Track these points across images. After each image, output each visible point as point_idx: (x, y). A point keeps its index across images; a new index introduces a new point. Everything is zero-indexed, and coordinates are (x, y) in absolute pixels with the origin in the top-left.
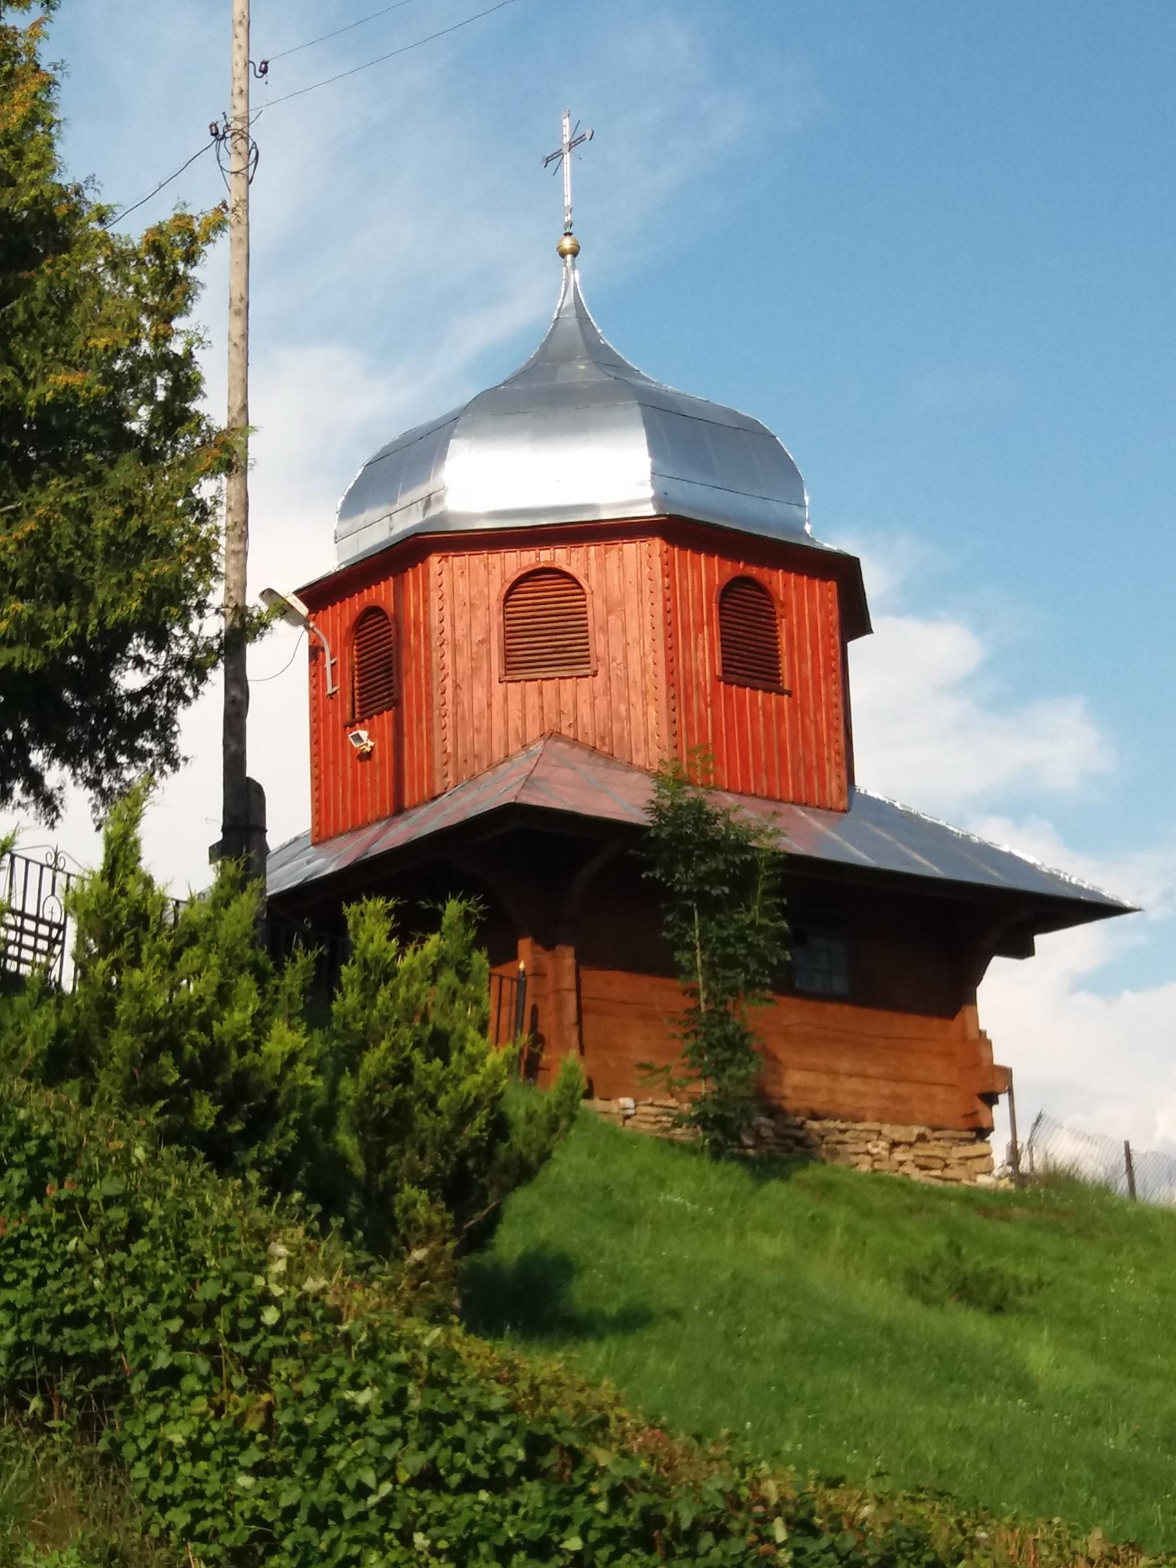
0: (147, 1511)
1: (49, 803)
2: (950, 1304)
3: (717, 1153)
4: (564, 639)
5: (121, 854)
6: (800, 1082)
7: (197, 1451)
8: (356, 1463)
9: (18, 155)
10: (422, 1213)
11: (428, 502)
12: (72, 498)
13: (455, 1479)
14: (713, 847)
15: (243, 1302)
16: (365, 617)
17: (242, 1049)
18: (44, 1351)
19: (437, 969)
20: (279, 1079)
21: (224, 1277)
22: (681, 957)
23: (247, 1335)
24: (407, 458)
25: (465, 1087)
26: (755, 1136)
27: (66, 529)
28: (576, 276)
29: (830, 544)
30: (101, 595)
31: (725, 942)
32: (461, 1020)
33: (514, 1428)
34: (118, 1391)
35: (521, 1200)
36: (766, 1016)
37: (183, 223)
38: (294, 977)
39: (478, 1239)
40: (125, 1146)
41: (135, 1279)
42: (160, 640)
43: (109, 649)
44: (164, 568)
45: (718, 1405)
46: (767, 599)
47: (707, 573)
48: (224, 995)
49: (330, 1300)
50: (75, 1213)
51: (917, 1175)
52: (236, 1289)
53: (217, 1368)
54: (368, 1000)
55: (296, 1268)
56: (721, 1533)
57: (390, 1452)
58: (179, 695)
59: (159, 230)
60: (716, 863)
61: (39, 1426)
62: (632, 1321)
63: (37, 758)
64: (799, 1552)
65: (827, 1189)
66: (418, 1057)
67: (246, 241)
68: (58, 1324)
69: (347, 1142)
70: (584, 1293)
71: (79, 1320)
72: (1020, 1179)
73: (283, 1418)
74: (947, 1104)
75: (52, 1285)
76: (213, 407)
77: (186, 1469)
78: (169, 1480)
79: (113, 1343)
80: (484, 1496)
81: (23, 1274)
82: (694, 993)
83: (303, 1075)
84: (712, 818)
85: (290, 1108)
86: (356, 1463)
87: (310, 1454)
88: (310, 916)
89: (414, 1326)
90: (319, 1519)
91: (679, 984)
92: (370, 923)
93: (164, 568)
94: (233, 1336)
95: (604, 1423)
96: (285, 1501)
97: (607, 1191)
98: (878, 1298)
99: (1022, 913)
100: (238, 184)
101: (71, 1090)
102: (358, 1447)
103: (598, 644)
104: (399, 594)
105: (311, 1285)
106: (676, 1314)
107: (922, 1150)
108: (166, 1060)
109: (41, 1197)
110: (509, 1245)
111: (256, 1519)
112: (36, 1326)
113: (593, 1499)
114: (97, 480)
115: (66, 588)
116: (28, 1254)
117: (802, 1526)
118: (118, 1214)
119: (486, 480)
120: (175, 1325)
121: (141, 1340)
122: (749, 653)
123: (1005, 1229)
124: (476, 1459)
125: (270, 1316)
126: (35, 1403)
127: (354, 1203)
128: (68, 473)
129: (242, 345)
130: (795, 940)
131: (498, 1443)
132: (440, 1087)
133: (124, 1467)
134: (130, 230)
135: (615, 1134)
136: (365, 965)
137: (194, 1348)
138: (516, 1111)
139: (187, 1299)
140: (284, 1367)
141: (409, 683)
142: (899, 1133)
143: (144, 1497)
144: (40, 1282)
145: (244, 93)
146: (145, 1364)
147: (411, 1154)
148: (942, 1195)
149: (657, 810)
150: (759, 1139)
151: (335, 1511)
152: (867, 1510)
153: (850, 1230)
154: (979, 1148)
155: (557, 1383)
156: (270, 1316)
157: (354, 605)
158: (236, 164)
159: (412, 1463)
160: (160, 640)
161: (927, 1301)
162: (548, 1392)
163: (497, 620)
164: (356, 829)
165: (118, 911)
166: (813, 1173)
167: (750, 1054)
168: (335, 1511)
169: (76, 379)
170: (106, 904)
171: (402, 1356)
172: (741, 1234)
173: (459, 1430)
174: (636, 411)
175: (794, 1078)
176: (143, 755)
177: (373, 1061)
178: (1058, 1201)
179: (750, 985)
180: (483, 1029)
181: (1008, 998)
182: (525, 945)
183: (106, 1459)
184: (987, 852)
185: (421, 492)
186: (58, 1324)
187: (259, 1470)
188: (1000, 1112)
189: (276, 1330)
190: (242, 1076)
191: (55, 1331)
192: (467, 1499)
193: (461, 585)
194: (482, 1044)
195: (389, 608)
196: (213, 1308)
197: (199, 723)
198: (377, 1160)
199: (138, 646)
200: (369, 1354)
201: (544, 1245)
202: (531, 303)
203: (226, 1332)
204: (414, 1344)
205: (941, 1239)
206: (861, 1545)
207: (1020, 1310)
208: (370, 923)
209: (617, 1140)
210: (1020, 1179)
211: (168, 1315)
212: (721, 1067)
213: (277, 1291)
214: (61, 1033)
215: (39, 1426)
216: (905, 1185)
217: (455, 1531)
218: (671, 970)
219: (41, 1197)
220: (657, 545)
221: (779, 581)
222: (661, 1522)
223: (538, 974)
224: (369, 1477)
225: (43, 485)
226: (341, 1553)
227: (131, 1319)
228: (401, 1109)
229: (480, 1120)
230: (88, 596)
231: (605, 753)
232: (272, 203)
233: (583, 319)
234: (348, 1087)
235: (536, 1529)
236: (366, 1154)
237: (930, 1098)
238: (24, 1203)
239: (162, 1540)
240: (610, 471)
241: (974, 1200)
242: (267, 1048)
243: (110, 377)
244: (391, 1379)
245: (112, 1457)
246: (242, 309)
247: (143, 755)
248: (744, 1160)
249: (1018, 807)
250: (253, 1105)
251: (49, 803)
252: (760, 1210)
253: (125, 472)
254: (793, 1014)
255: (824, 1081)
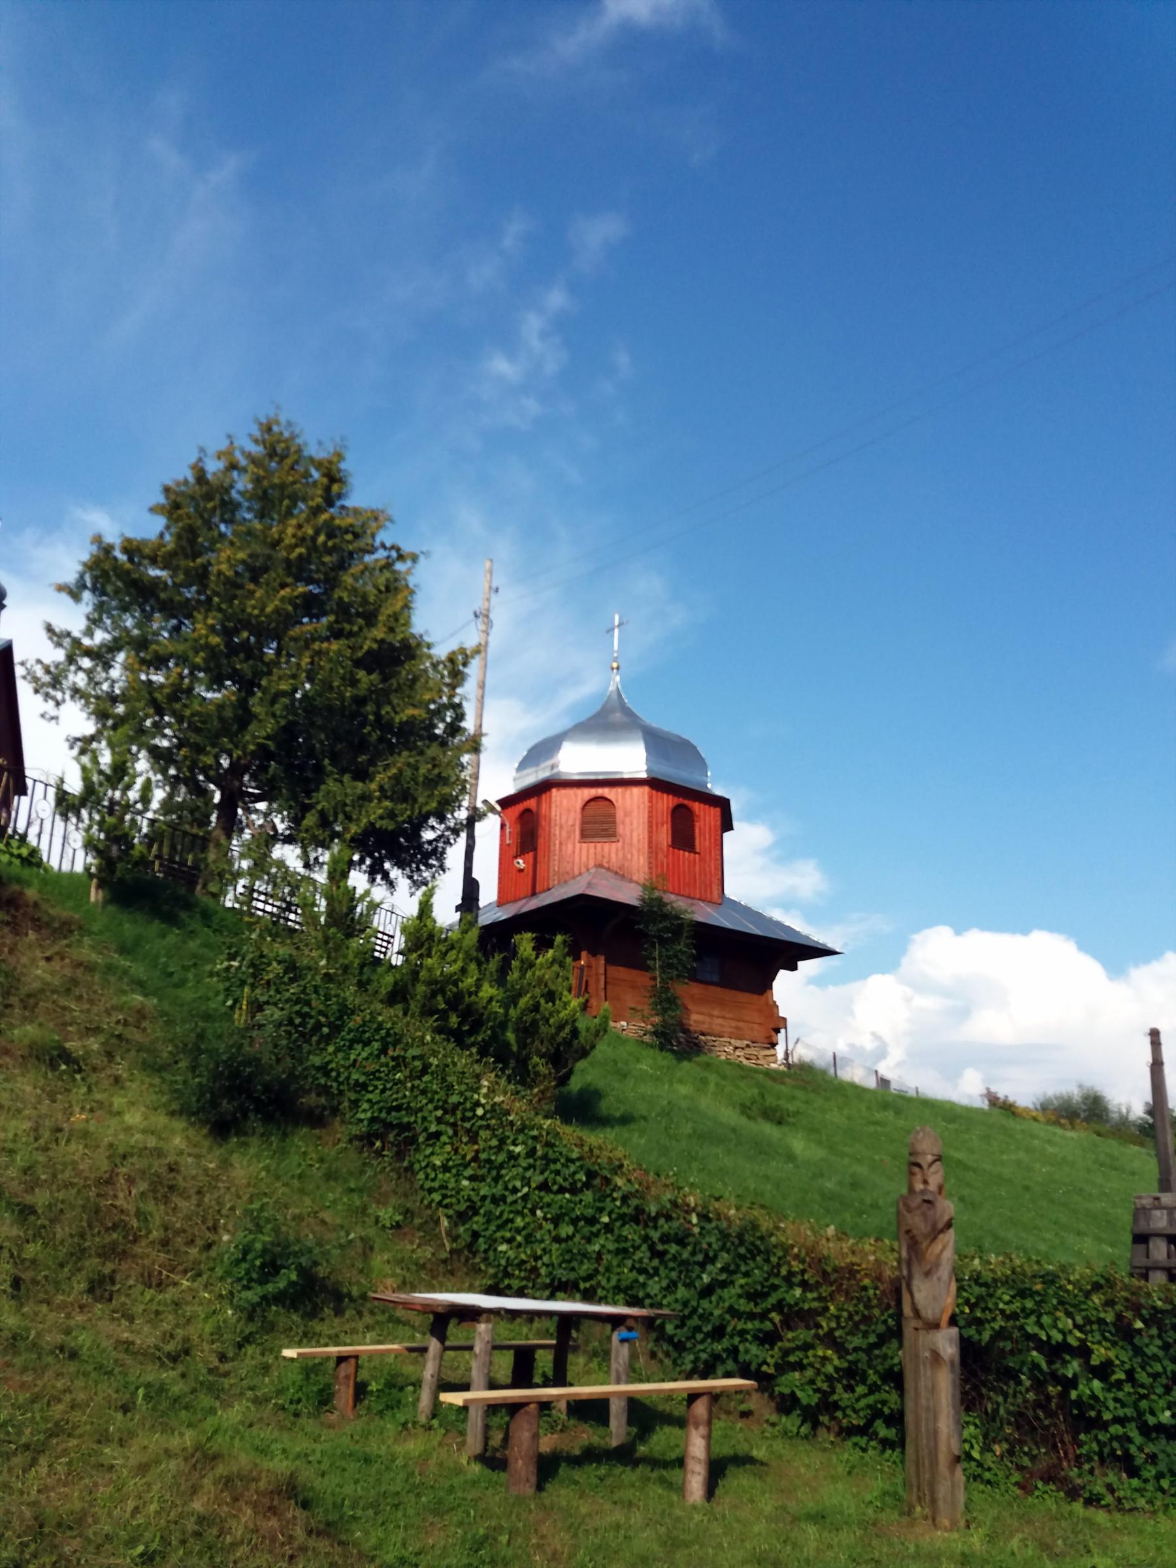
0: (422, 1193)
1: (391, 884)
2: (760, 1120)
3: (662, 1048)
4: (605, 826)
5: (425, 908)
6: (697, 1019)
7: (446, 1168)
8: (514, 1178)
9: (397, 620)
10: (543, 1070)
11: (553, 767)
12: (412, 760)
13: (555, 1188)
14: (666, 917)
15: (468, 1105)
16: (525, 811)
17: (470, 994)
18: (383, 1121)
19: (552, 963)
20: (485, 1008)
21: (461, 1094)
22: (650, 963)
23: (469, 1119)
24: (545, 749)
25: (562, 1015)
26: (678, 1042)
27: (408, 773)
28: (618, 678)
29: (718, 792)
30: (421, 800)
31: (669, 957)
32: (559, 986)
33: (581, 1167)
34: (413, 1141)
35: (581, 1065)
36: (686, 990)
37: (462, 651)
38: (493, 964)
39: (563, 1080)
40: (422, 1036)
41: (424, 1092)
42: (442, 819)
43: (420, 823)
44: (446, 790)
45: (662, 1159)
46: (691, 814)
47: (666, 802)
48: (463, 970)
49: (505, 1106)
50: (400, 1062)
51: (745, 1062)
52: (466, 1099)
53: (456, 1133)
54: (523, 976)
55: (492, 1091)
56: (669, 1218)
57: (528, 1174)
58: (448, 842)
59: (453, 653)
60: (667, 924)
61: (379, 1153)
62: (626, 1120)
63: (387, 865)
64: (702, 1228)
65: (707, 1066)
66: (542, 1001)
67: (485, 659)
68: (390, 1110)
69: (510, 1036)
70: (606, 1106)
71: (398, 1108)
72: (788, 1066)
73: (483, 1156)
74: (759, 1033)
75: (388, 1093)
76: (469, 724)
77: (440, 1176)
78: (433, 1180)
79: (412, 1119)
80: (567, 1196)
81: (376, 1087)
82: (654, 979)
83: (496, 1007)
84: (666, 905)
85: (489, 1020)
86: (514, 1178)
87: (494, 1173)
88: (497, 938)
89: (539, 1120)
90: (496, 1200)
91: (649, 974)
92: (525, 942)
93: (446, 790)
94: (464, 1119)
95: (621, 1166)
96: (482, 1193)
97: (615, 1062)
98: (729, 1116)
99: (794, 952)
100: (483, 635)
101: (398, 1009)
102: (514, 1171)
103: (620, 829)
104: (539, 804)
105: (498, 1099)
106: (645, 1118)
107: (748, 1051)
108: (440, 998)
109: (386, 1054)
110: (575, 1084)
111: (469, 1199)
112: (380, 1110)
113: (614, 1200)
114: (421, 753)
115: (406, 797)
116: (379, 1079)
117: (704, 1217)
118: (417, 1063)
119: (579, 759)
120: (439, 1113)
121: (424, 1119)
122: (683, 834)
123: (783, 1088)
124: (565, 1180)
125: (480, 1112)
126: (378, 1144)
127: (512, 1063)
128: (410, 750)
129: (481, 701)
130: (696, 958)
131: (575, 1173)
132: (551, 1014)
133: (414, 1174)
134: (441, 652)
135: (619, 1038)
136: (522, 961)
137: (447, 1123)
138: (581, 1025)
139: (446, 1102)
140: (484, 1134)
141: (541, 841)
142: (738, 1043)
143: (422, 1187)
144: (383, 1091)
145: (488, 600)
146: (426, 1129)
147: (537, 1043)
148: (756, 1071)
149: (643, 900)
150: (679, 1042)
151: (503, 1199)
152: (732, 1212)
153: (717, 1084)
154: (771, 1052)
155: (600, 1148)
156: (480, 1112)
157: (519, 808)
158: (483, 627)
159: (537, 1179)
160: (442, 819)
161: (749, 1118)
162: (596, 1152)
163: (579, 816)
164: (515, 901)
165: (422, 934)
166: (702, 1058)
167: (677, 1006)
168: (503, 1199)
169: (416, 712)
170: (418, 930)
171: (535, 1133)
172: (671, 1083)
173: (558, 1166)
174: (640, 735)
175: (694, 1017)
176: (432, 866)
177: (523, 1002)
178: (808, 1078)
179: (679, 976)
180: (570, 991)
181: (789, 988)
182: (584, 954)
183: (406, 1169)
184: (779, 925)
185: (549, 763)
186: (390, 1110)
187: (472, 1178)
188: (781, 1037)
189: (482, 1118)
190: (470, 1006)
191: (388, 1113)
192: (560, 1196)
193: (565, 802)
194: (570, 997)
195: (534, 809)
196: (456, 1106)
197: (455, 855)
198: (522, 1045)
199: (432, 821)
200: (521, 1130)
201: (589, 1085)
202: (596, 683)
203: (460, 1117)
204: (540, 1128)
205: (756, 1091)
206: (729, 1226)
207: (789, 1124)
208: (525, 942)
209: (620, 1040)
210: (788, 1066)
211: (436, 1108)
212: (665, 1010)
213: (483, 1101)
214: (396, 983)
215: (379, 1153)
216: (740, 1066)
217: (554, 1210)
218: (647, 969)
219: (386, 1054)
220: (646, 789)
221: (697, 807)
222: (643, 1211)
223: (589, 967)
224: (518, 1184)
225: (399, 754)
226: (505, 1217)
227: (421, 1109)
228: (534, 1023)
229: (567, 1029)
230: (415, 800)
231: (621, 874)
232: (494, 641)
233: (619, 695)
234: (513, 1013)
235: (589, 1212)
236: (518, 1042)
237: (752, 1029)
238: (378, 1057)
239: (429, 1206)
240: (629, 758)
241: (770, 1075)
242: (481, 994)
243: (429, 711)
244: (530, 1142)
245: (410, 1168)
246: (482, 686)
247: (432, 866)
248: (673, 1051)
249: (787, 905)
250: (473, 1018)
251: (391, 884)
252: (679, 1074)
253: (433, 751)
254: (695, 989)
255: (707, 1019)
